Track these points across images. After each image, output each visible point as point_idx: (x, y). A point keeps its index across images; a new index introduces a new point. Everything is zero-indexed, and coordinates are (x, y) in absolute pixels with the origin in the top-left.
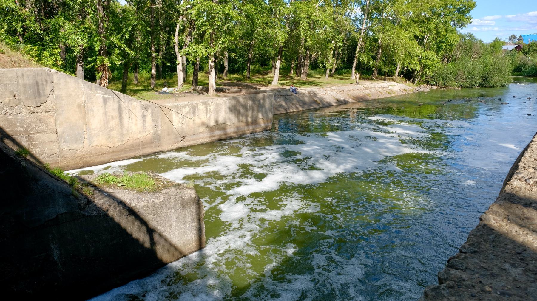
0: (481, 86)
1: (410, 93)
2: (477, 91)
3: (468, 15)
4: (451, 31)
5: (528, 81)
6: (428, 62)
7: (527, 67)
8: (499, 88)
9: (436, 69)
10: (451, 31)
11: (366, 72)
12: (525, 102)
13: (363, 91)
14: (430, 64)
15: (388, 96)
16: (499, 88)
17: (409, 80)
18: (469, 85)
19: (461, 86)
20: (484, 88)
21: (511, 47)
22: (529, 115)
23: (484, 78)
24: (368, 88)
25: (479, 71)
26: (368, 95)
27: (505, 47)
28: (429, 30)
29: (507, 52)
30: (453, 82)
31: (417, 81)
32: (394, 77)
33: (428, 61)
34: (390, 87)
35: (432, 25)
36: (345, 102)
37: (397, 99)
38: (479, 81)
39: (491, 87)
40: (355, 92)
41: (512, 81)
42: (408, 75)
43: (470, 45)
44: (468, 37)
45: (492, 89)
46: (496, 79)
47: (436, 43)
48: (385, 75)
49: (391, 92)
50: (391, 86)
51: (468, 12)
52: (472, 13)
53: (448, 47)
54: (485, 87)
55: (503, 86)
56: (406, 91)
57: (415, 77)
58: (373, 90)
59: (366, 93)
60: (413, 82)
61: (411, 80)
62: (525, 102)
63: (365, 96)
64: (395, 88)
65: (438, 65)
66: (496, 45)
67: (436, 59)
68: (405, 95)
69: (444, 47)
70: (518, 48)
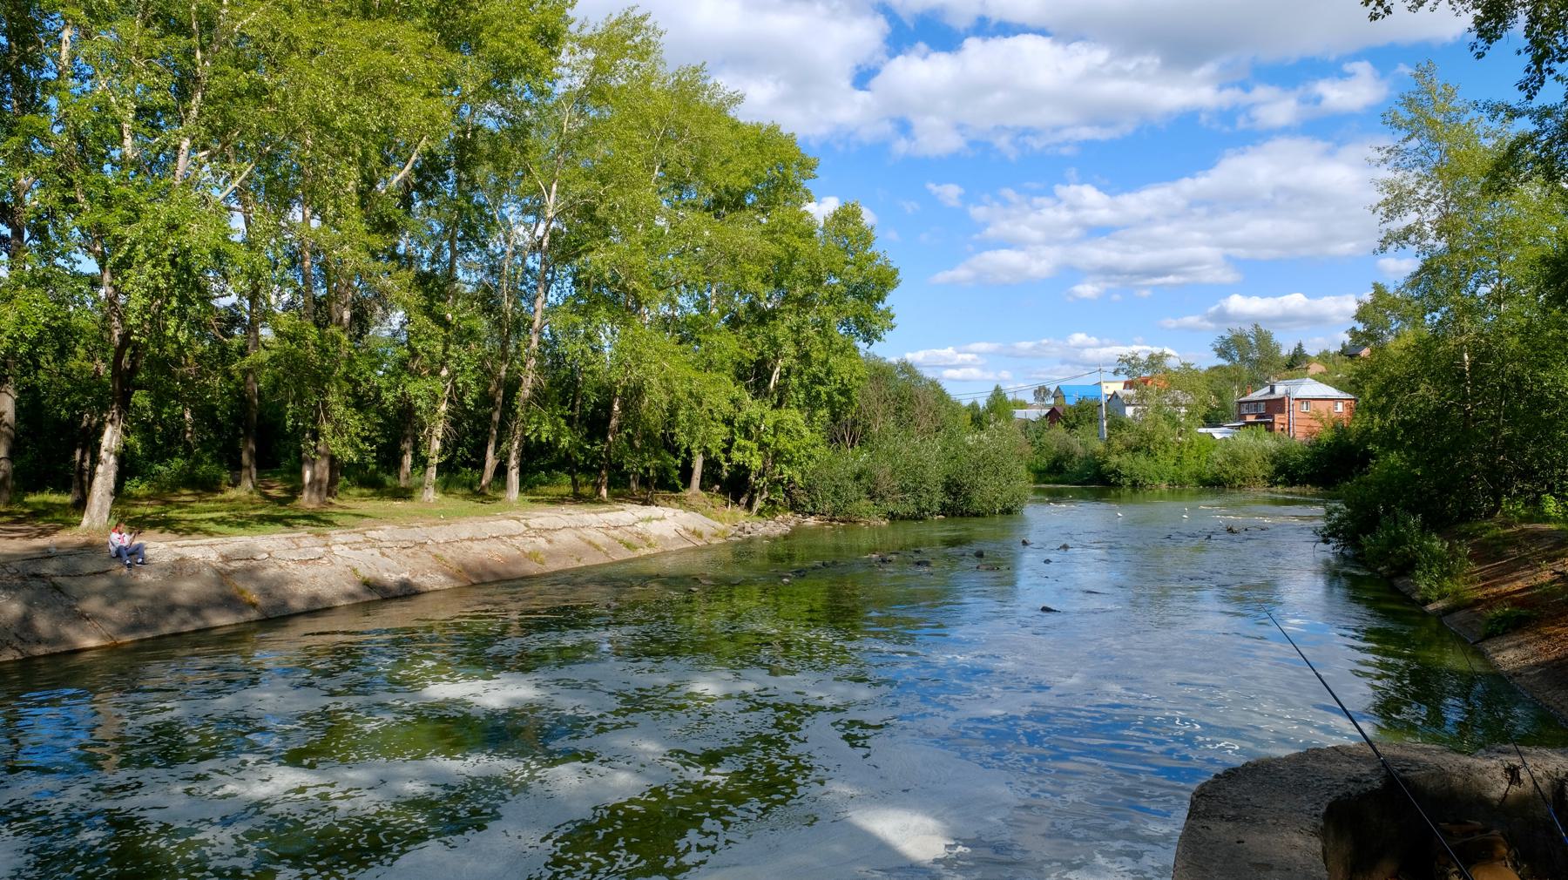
0: (949, 511)
1: (715, 542)
2: (938, 529)
3: (881, 306)
4: (842, 351)
5: (1083, 497)
6: (783, 442)
7: (1075, 459)
8: (998, 518)
9: (812, 465)
10: (842, 351)
11: (542, 468)
12: (1047, 561)
13: (517, 542)
14: (789, 446)
15: (627, 554)
16: (998, 518)
17: (736, 500)
18: (912, 509)
19: (893, 517)
20: (957, 519)
21: (1034, 414)
22: (1045, 609)
23: (952, 487)
24: (541, 531)
25: (935, 474)
26: (531, 556)
27: (1020, 414)
28: (774, 343)
29: (1026, 425)
30: (864, 504)
31: (758, 504)
32: (688, 493)
33: (783, 438)
34: (640, 525)
35: (782, 330)
36: (408, 592)
37: (669, 565)
38: (938, 497)
39: (977, 515)
40: (477, 547)
41: (1031, 497)
42: (736, 486)
43: (910, 397)
44: (902, 371)
45: (976, 520)
46: (987, 490)
47: (801, 385)
48: (662, 485)
49: (635, 541)
50: (650, 520)
51: (880, 299)
52: (892, 300)
53: (837, 397)
54: (962, 515)
55: (1008, 511)
56: (700, 535)
57: (754, 491)
58: (565, 538)
59: (528, 548)
60: (749, 506)
61: (743, 500)
62: (1047, 561)
63: (517, 562)
64: (667, 528)
65: (816, 453)
66: (999, 404)
67: (806, 432)
68: (698, 549)
69: (824, 397)
70: (1053, 415)
